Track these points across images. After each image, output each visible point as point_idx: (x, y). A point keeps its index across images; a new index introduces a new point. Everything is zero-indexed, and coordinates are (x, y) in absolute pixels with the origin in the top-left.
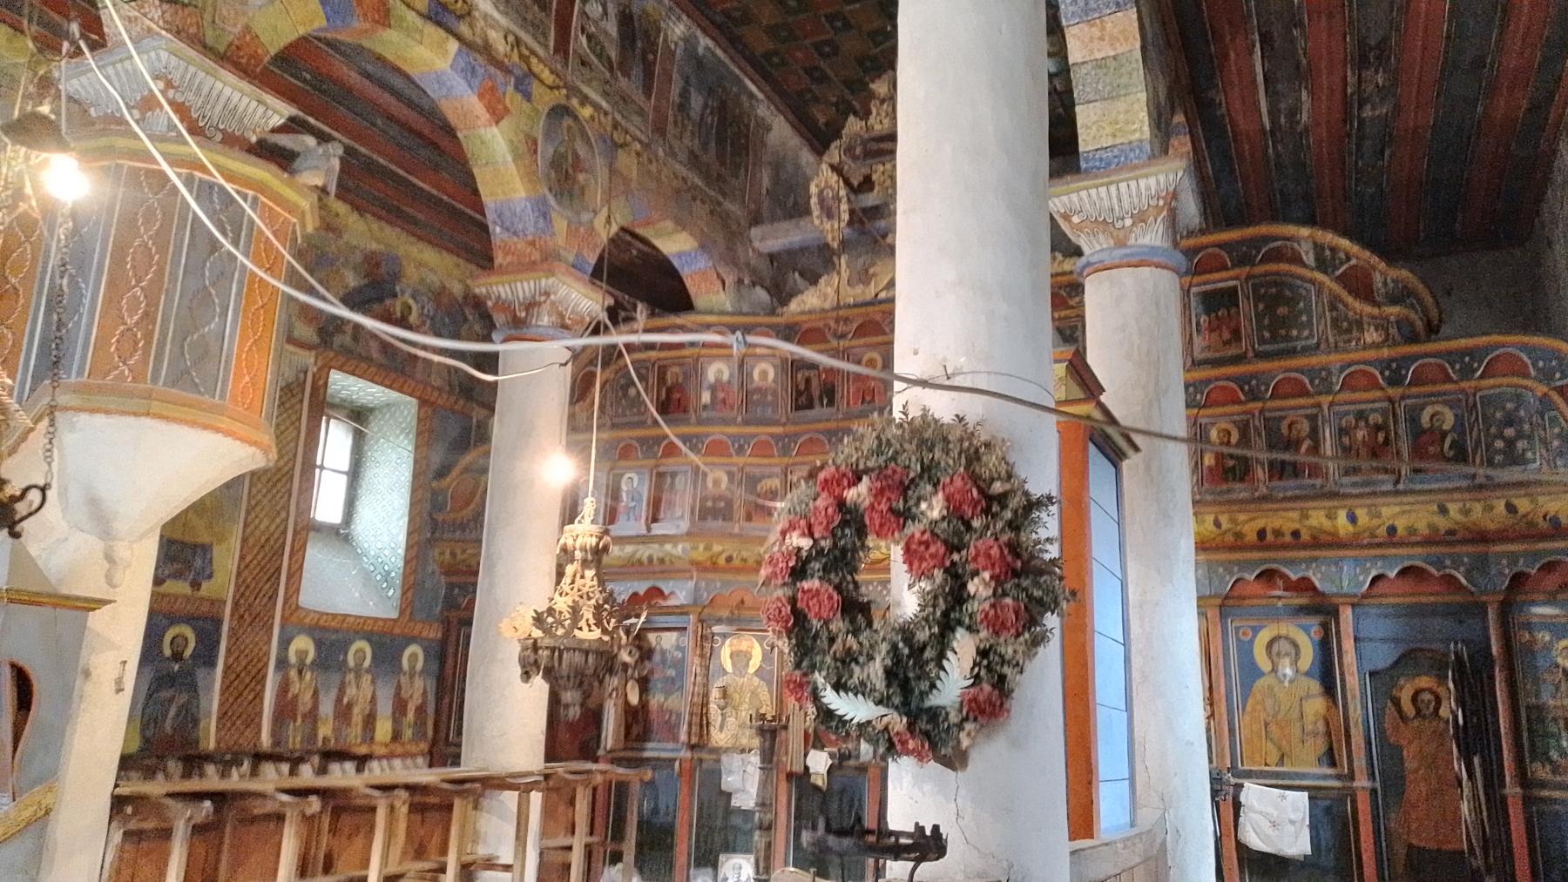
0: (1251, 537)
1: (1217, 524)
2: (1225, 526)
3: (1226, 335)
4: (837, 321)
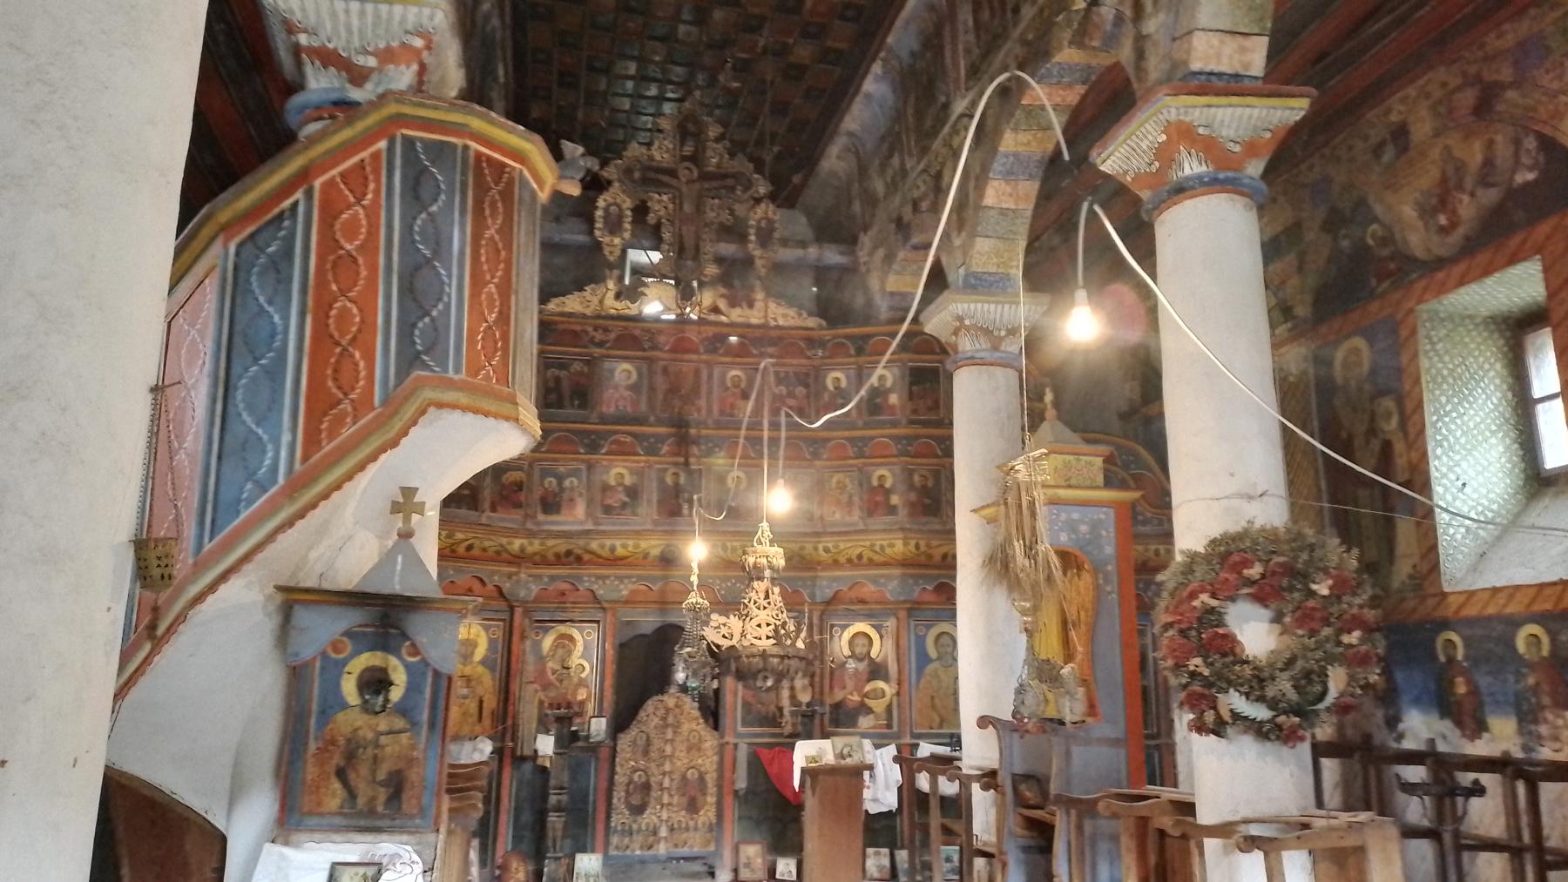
0: (937, 558)
1: (917, 547)
2: (923, 549)
3: (929, 402)
4: (596, 329)
